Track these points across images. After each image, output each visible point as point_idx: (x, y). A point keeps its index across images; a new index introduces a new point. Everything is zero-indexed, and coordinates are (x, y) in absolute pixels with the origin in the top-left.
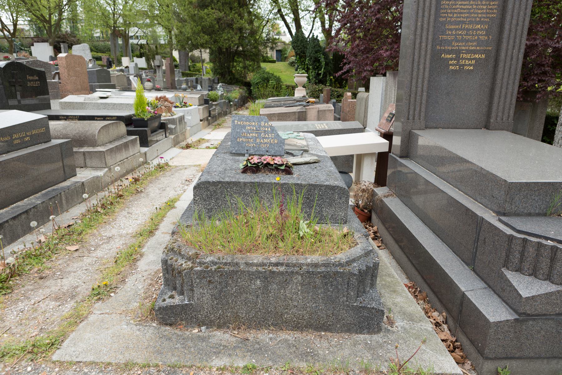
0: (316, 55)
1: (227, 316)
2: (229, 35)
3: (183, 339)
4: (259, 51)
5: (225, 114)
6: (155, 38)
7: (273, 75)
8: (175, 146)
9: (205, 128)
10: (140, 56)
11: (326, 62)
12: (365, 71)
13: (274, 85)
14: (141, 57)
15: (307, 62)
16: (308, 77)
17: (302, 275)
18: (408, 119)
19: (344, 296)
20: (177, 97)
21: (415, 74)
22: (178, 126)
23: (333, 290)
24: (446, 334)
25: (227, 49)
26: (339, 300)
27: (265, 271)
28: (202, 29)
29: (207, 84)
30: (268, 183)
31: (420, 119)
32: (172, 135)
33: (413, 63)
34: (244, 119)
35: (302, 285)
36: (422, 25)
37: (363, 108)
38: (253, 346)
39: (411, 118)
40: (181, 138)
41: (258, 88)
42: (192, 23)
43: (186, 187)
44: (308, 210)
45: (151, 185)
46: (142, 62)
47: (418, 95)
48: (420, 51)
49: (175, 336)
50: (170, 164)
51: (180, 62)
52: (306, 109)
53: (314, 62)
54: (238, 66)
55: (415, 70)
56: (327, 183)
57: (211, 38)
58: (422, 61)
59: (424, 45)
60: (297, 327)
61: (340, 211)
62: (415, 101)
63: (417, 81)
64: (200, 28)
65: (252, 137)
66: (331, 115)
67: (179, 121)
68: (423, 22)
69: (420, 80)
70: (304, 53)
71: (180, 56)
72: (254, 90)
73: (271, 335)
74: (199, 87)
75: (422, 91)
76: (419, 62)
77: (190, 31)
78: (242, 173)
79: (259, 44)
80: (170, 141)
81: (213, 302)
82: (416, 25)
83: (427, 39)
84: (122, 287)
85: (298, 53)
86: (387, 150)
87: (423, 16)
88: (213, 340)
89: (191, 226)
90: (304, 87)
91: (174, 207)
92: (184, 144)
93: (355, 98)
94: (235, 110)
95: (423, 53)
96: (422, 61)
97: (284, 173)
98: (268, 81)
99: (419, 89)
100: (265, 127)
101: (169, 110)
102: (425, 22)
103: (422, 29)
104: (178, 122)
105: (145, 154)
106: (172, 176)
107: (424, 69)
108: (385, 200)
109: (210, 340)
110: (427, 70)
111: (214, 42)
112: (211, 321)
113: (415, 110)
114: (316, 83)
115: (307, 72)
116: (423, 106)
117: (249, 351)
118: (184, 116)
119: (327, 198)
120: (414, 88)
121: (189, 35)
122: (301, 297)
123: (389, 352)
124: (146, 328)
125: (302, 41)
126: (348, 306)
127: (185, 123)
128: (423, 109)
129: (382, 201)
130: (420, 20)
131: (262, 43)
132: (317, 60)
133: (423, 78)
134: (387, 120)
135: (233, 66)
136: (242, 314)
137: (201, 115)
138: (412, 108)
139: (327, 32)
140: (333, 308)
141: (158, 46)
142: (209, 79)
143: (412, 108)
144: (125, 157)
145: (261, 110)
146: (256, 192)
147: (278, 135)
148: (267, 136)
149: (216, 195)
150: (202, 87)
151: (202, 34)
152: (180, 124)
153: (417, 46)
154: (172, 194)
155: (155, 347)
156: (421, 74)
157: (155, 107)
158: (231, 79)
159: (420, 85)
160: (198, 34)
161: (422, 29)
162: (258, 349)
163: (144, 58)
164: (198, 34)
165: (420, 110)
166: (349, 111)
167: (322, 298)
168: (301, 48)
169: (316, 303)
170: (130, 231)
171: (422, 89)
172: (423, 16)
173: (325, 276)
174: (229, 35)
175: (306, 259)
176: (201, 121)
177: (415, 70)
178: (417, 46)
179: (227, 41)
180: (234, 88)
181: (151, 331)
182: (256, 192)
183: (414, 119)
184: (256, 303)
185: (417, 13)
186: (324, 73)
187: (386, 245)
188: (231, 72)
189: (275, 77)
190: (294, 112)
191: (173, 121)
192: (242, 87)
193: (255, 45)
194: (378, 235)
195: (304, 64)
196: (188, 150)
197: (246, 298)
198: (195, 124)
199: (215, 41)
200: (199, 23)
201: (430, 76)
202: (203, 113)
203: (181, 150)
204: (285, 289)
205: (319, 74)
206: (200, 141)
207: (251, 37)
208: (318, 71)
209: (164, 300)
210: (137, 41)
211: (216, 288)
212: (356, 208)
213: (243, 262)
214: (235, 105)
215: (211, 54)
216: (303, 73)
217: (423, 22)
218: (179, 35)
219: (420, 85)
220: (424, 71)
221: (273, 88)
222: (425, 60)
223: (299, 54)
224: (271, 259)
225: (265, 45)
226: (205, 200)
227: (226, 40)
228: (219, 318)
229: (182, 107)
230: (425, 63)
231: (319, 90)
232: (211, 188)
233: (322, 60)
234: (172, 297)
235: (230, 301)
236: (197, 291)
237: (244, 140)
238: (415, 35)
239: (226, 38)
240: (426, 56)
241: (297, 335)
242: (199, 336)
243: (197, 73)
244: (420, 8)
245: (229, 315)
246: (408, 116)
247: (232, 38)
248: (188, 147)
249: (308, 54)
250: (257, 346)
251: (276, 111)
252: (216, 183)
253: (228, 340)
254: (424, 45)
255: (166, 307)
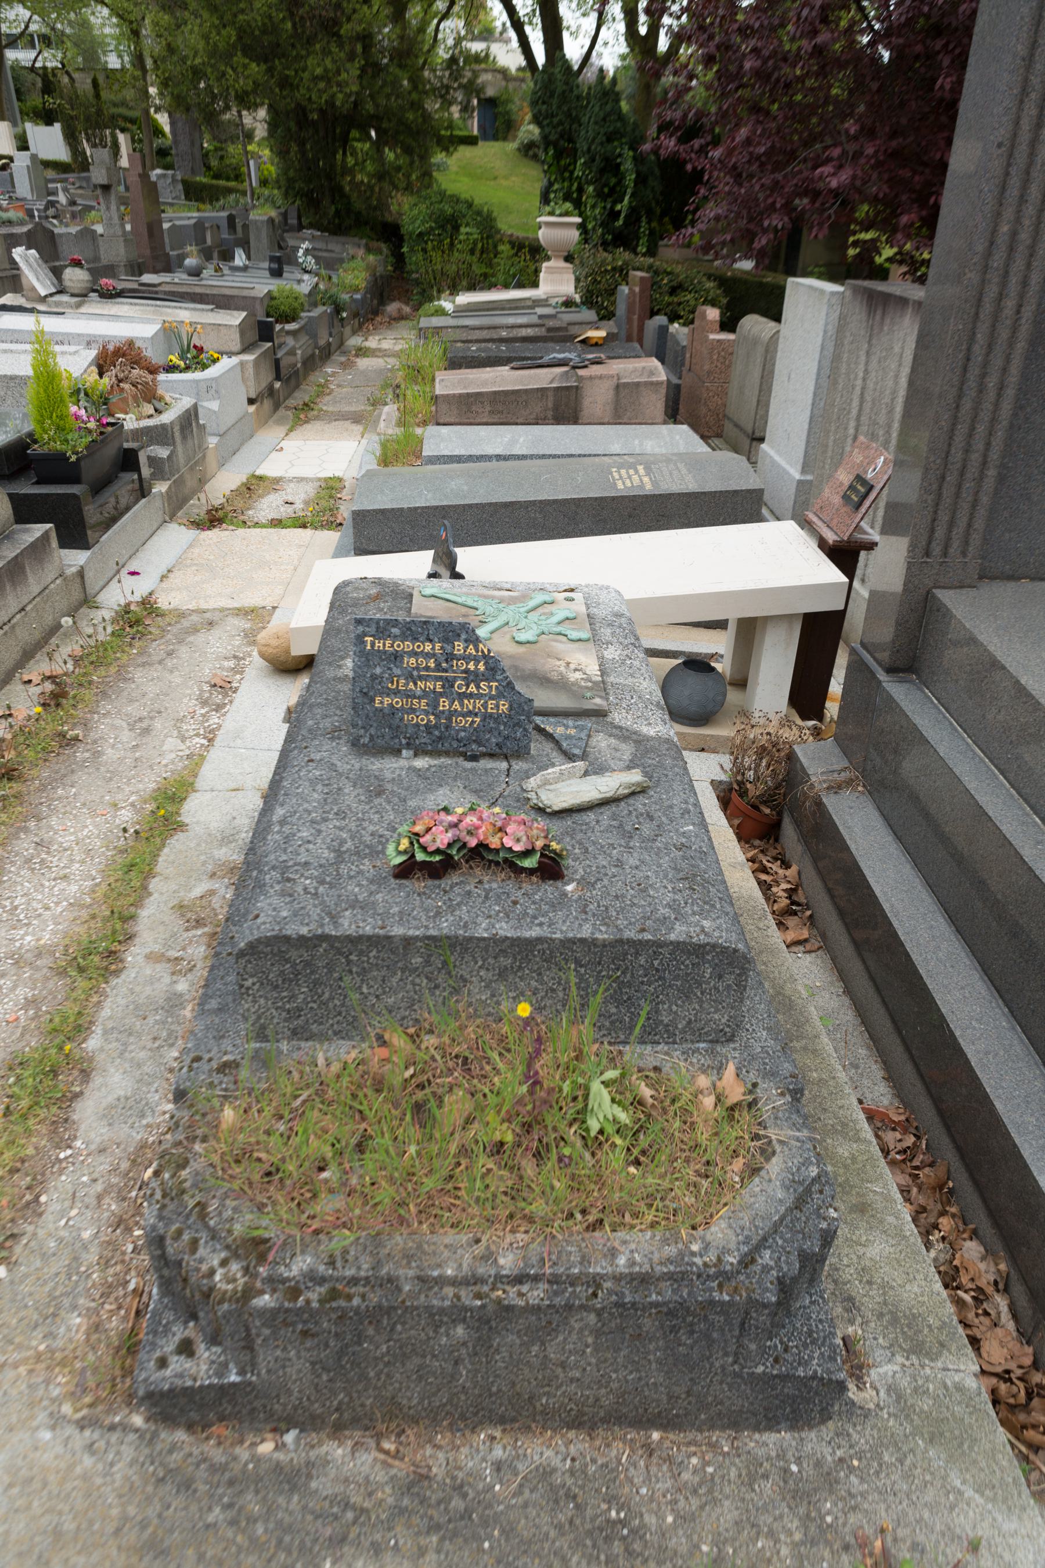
0: (609, 147)
1: (363, 1405)
2: (328, 62)
3: (231, 1483)
4: (426, 117)
5: (326, 354)
6: (89, 48)
7: (470, 205)
8: (172, 516)
9: (263, 422)
10: (47, 118)
11: (638, 174)
12: (765, 231)
13: (475, 243)
14: (49, 122)
15: (578, 173)
16: (582, 227)
17: (599, 1313)
18: (927, 554)
19: (726, 1354)
20: (169, 332)
21: (967, 405)
22: (180, 449)
23: (696, 1342)
24: (1003, 1347)
25: (322, 112)
26: (712, 1365)
27: (483, 1306)
28: (240, 38)
29: (261, 240)
30: (484, 939)
31: (964, 554)
32: (164, 479)
33: (965, 369)
34: (395, 631)
35: (598, 1333)
36: (1014, 234)
37: (756, 374)
38: (444, 1501)
39: (937, 549)
40: (190, 482)
41: (424, 250)
42: (206, 15)
43: (214, 719)
44: (614, 1010)
45: (105, 706)
46: (49, 141)
47: (969, 475)
48: (993, 326)
49: (202, 1472)
50: (163, 602)
51: (175, 141)
52: (580, 379)
53: (602, 171)
54: (361, 156)
55: (971, 393)
56: (678, 933)
57: (270, 70)
58: (997, 362)
59: (1010, 304)
60: (581, 1421)
61: (717, 1011)
62: (957, 495)
63: (972, 428)
64: (230, 33)
65: (425, 694)
66: (657, 403)
67: (183, 429)
68: (1018, 220)
69: (981, 429)
70: (570, 140)
71: (172, 124)
72: (415, 259)
73: (498, 1453)
74: (240, 258)
75: (984, 463)
76: (985, 364)
77: (201, 45)
78: (397, 876)
79: (426, 93)
80: (158, 503)
81: (319, 1376)
82: (994, 231)
83: (1025, 283)
84: (30, 1229)
85: (553, 137)
86: (842, 608)
87: (1022, 199)
88: (322, 1485)
89: (234, 1065)
90: (569, 259)
91: (181, 827)
92: (198, 507)
93: (733, 330)
94: (354, 332)
95: (1004, 334)
96: (997, 362)
97: (534, 879)
98: (456, 228)
99: (975, 457)
100: (467, 658)
101: (150, 395)
102: (1027, 222)
103: (1011, 249)
104: (177, 434)
105: (81, 574)
106: (169, 663)
107: (1001, 388)
108: (830, 802)
109: (314, 1485)
110: (1010, 392)
111: (282, 87)
112: (313, 1417)
113: (952, 524)
114: (605, 245)
115: (578, 205)
116: (982, 512)
117: (434, 1527)
118: (195, 407)
119: (677, 978)
120: (957, 455)
121: (198, 61)
122: (593, 1360)
123: (854, 1508)
124: (114, 1437)
125: (564, 97)
126: (736, 1375)
127: (202, 428)
128: (979, 524)
129: (819, 804)
130: (1009, 213)
131: (434, 90)
132: (611, 166)
133: (994, 420)
134: (846, 497)
135: (346, 171)
136: (412, 1397)
137: (251, 383)
138: (944, 517)
139: (641, 45)
140: (691, 1380)
141: (103, 79)
142: (271, 220)
143: (944, 517)
144: (13, 610)
145: (440, 376)
146: (445, 963)
147: (510, 685)
148: (472, 688)
149: (312, 973)
150: (249, 258)
151: (239, 59)
152: (184, 438)
153: (988, 307)
154: (169, 751)
155: (143, 1525)
156: (987, 406)
157: (103, 402)
158: (337, 212)
159: (979, 445)
160: (227, 56)
161: (1011, 249)
162: (462, 1518)
163: (57, 126)
164: (227, 56)
165: (969, 525)
166: (709, 373)
167: (659, 1362)
168: (561, 123)
169: (638, 1370)
170: (46, 938)
171: (985, 456)
172: (1022, 199)
173: (673, 1315)
174: (328, 62)
175: (613, 1253)
176: (251, 401)
177: (971, 393)
178: (988, 307)
179: (322, 85)
180: (351, 251)
181: (128, 1452)
182: (445, 963)
183: (945, 554)
184: (454, 1377)
185: (1003, 188)
186: (633, 211)
187: (823, 936)
188: (340, 189)
189: (479, 213)
190: (543, 391)
191: (160, 435)
192: (375, 244)
193: (415, 96)
194: (800, 897)
195: (571, 178)
196: (213, 535)
197: (421, 1367)
198: (230, 421)
199: (285, 83)
200: (228, 17)
201: (1018, 407)
202: (257, 373)
203: (193, 533)
204: (543, 1343)
205: (614, 215)
206: (254, 487)
207: (401, 66)
208: (615, 203)
209: (163, 1363)
210: (32, 54)
211: (327, 1346)
212: (735, 796)
213: (411, 1273)
214: (356, 315)
215: (273, 126)
216: (567, 214)
217: (1018, 220)
218: (164, 60)
219: (979, 445)
220: (999, 395)
221: (472, 252)
222: (1008, 360)
223: (555, 145)
224: (502, 1261)
225: (444, 94)
226: (277, 987)
227: (320, 78)
228: (337, 1410)
229: (187, 368)
230: (1005, 370)
231: (614, 269)
232: (293, 954)
233: (628, 165)
234: (186, 1348)
235: (372, 1374)
236: (266, 1358)
237: (398, 702)
238: (986, 268)
239: (319, 71)
240: (1011, 344)
241: (579, 1444)
242: (278, 1468)
243: (232, 184)
244: (1013, 171)
245: (368, 1402)
246: (929, 543)
247: (338, 72)
248: (214, 519)
249: (582, 145)
250: (457, 1504)
251: (485, 383)
252: (310, 939)
253: (367, 1478)
254: (1010, 304)
255: (171, 1391)
